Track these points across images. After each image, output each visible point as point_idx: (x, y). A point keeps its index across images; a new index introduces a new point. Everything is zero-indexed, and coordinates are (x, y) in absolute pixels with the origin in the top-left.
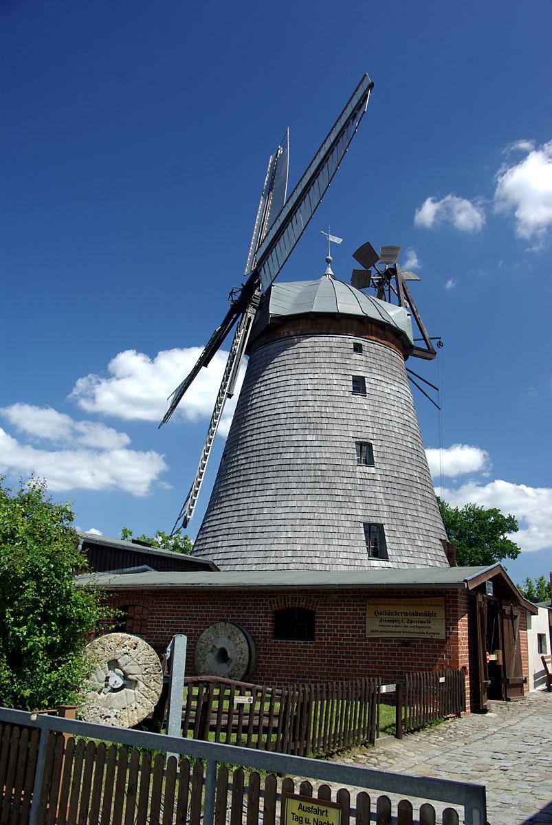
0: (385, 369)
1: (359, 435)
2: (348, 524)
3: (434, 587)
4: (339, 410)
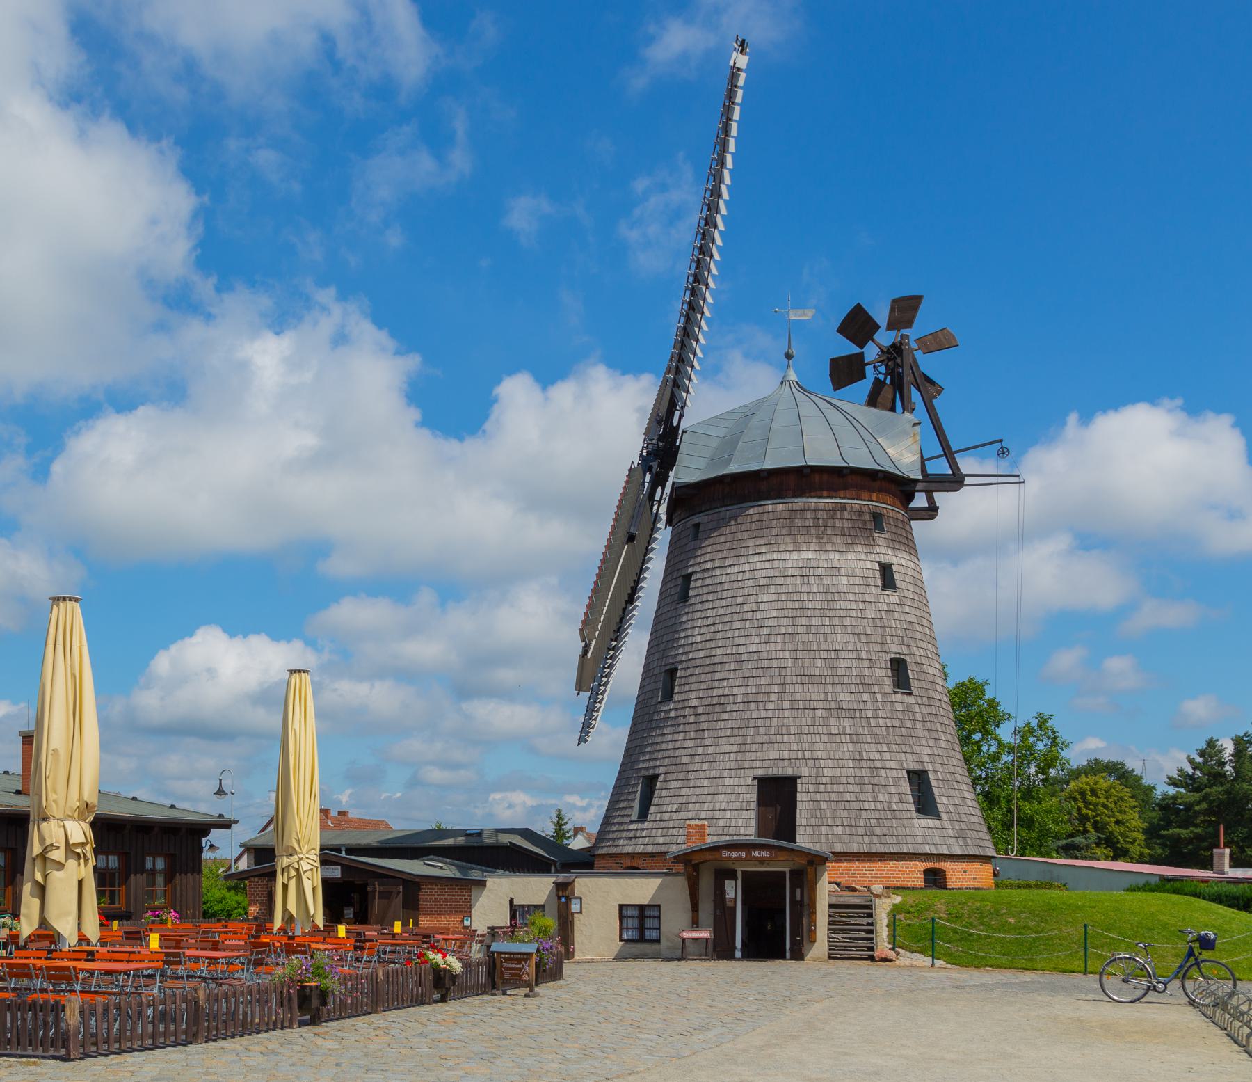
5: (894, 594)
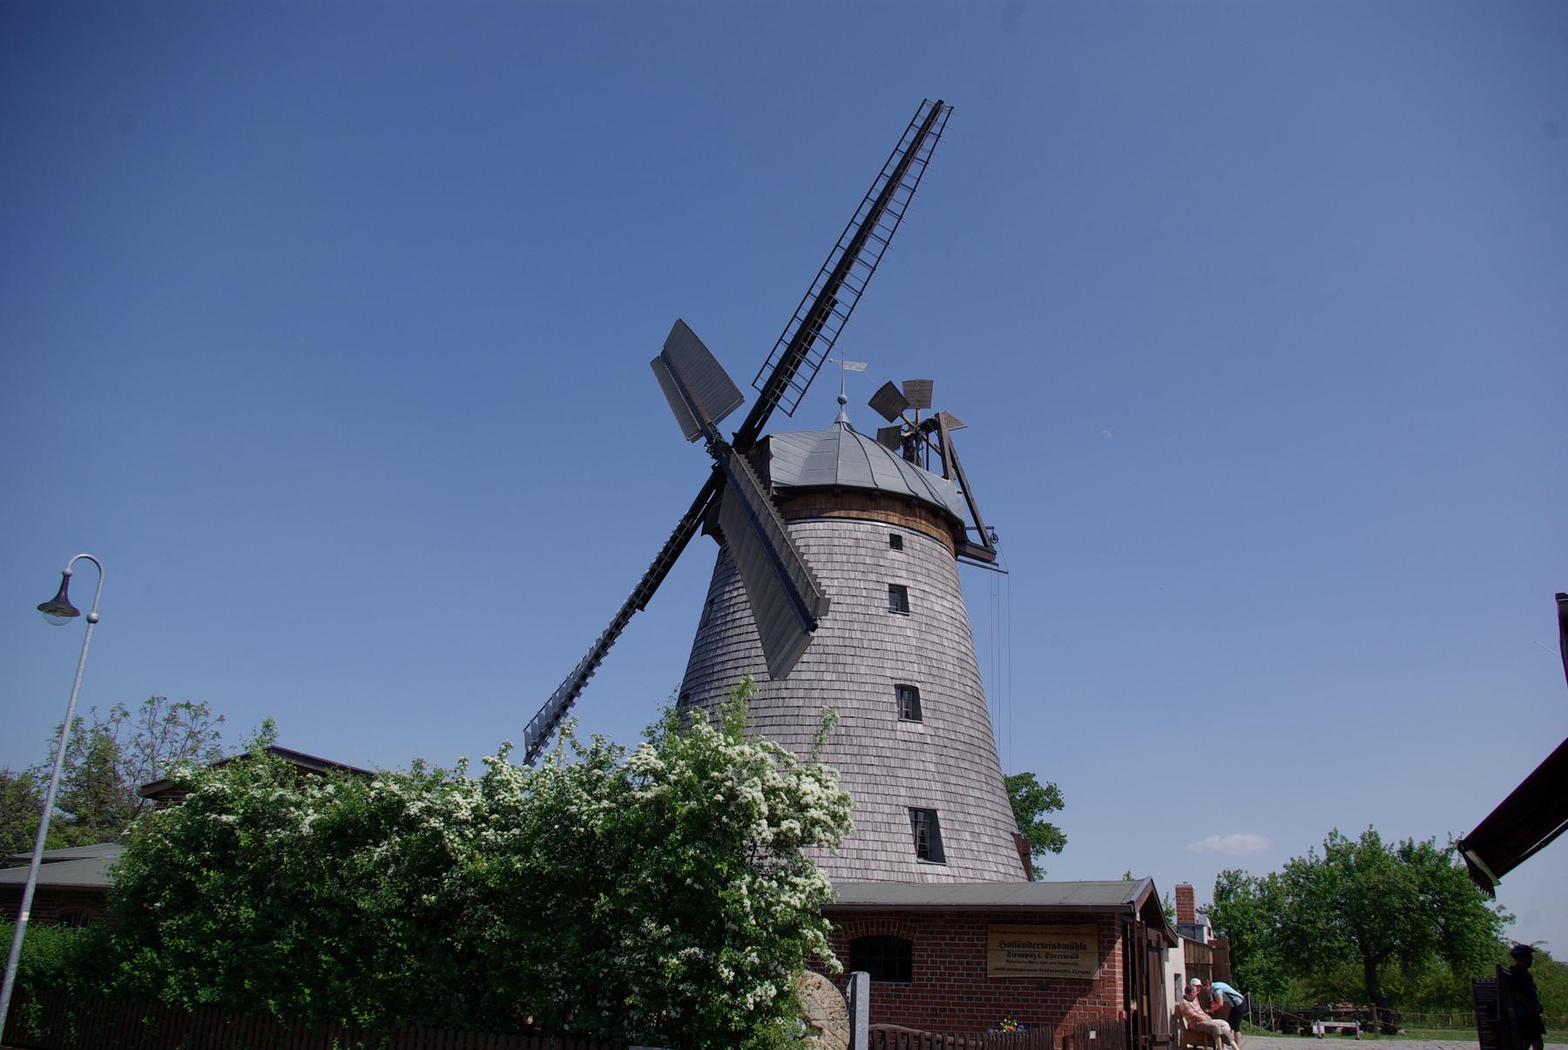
0: (933, 575)
1: (901, 674)
2: (887, 809)
3: (1090, 910)
4: (870, 636)
5: (906, 617)
